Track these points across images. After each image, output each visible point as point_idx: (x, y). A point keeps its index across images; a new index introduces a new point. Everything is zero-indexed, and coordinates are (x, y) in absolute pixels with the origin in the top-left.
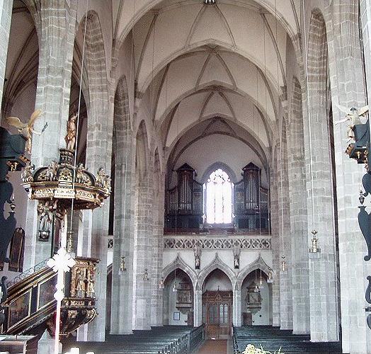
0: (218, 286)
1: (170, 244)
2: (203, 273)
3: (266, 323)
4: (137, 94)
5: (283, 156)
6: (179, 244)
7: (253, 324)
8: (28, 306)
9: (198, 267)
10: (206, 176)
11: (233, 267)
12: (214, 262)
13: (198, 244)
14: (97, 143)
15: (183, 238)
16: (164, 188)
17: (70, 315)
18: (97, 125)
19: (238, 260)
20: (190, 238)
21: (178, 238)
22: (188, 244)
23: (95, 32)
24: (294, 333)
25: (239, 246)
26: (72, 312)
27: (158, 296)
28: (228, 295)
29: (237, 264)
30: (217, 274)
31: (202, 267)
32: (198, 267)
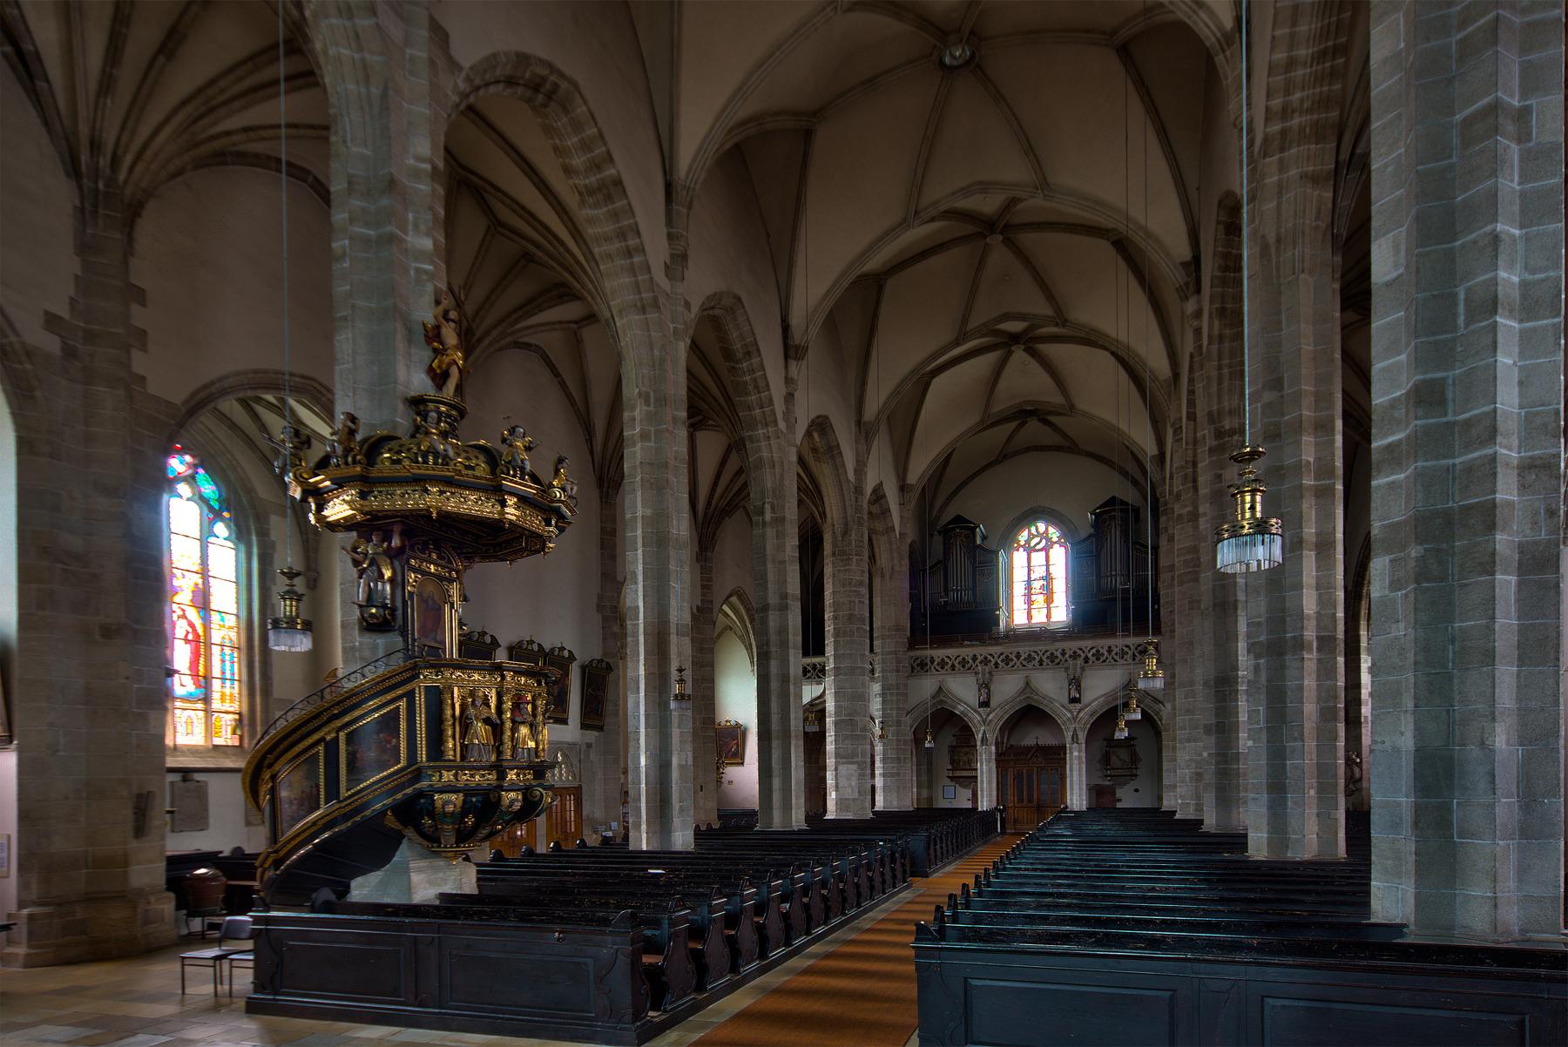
0: (1035, 737)
1: (922, 666)
2: (997, 716)
3: (1146, 803)
4: (792, 353)
5: (1190, 453)
6: (943, 664)
7: (1119, 805)
8: (318, 786)
9: (985, 704)
10: (1007, 540)
11: (1066, 701)
12: (1022, 692)
13: (985, 661)
14: (644, 436)
15: (951, 652)
16: (906, 562)
17: (506, 802)
18: (640, 394)
19: (1079, 686)
20: (966, 652)
21: (939, 653)
22: (964, 662)
23: (585, 146)
24: (1204, 828)
25: (1080, 662)
26: (512, 795)
27: (898, 759)
28: (1056, 755)
29: (1075, 694)
30: (1030, 713)
31: (993, 703)
32: (985, 704)
